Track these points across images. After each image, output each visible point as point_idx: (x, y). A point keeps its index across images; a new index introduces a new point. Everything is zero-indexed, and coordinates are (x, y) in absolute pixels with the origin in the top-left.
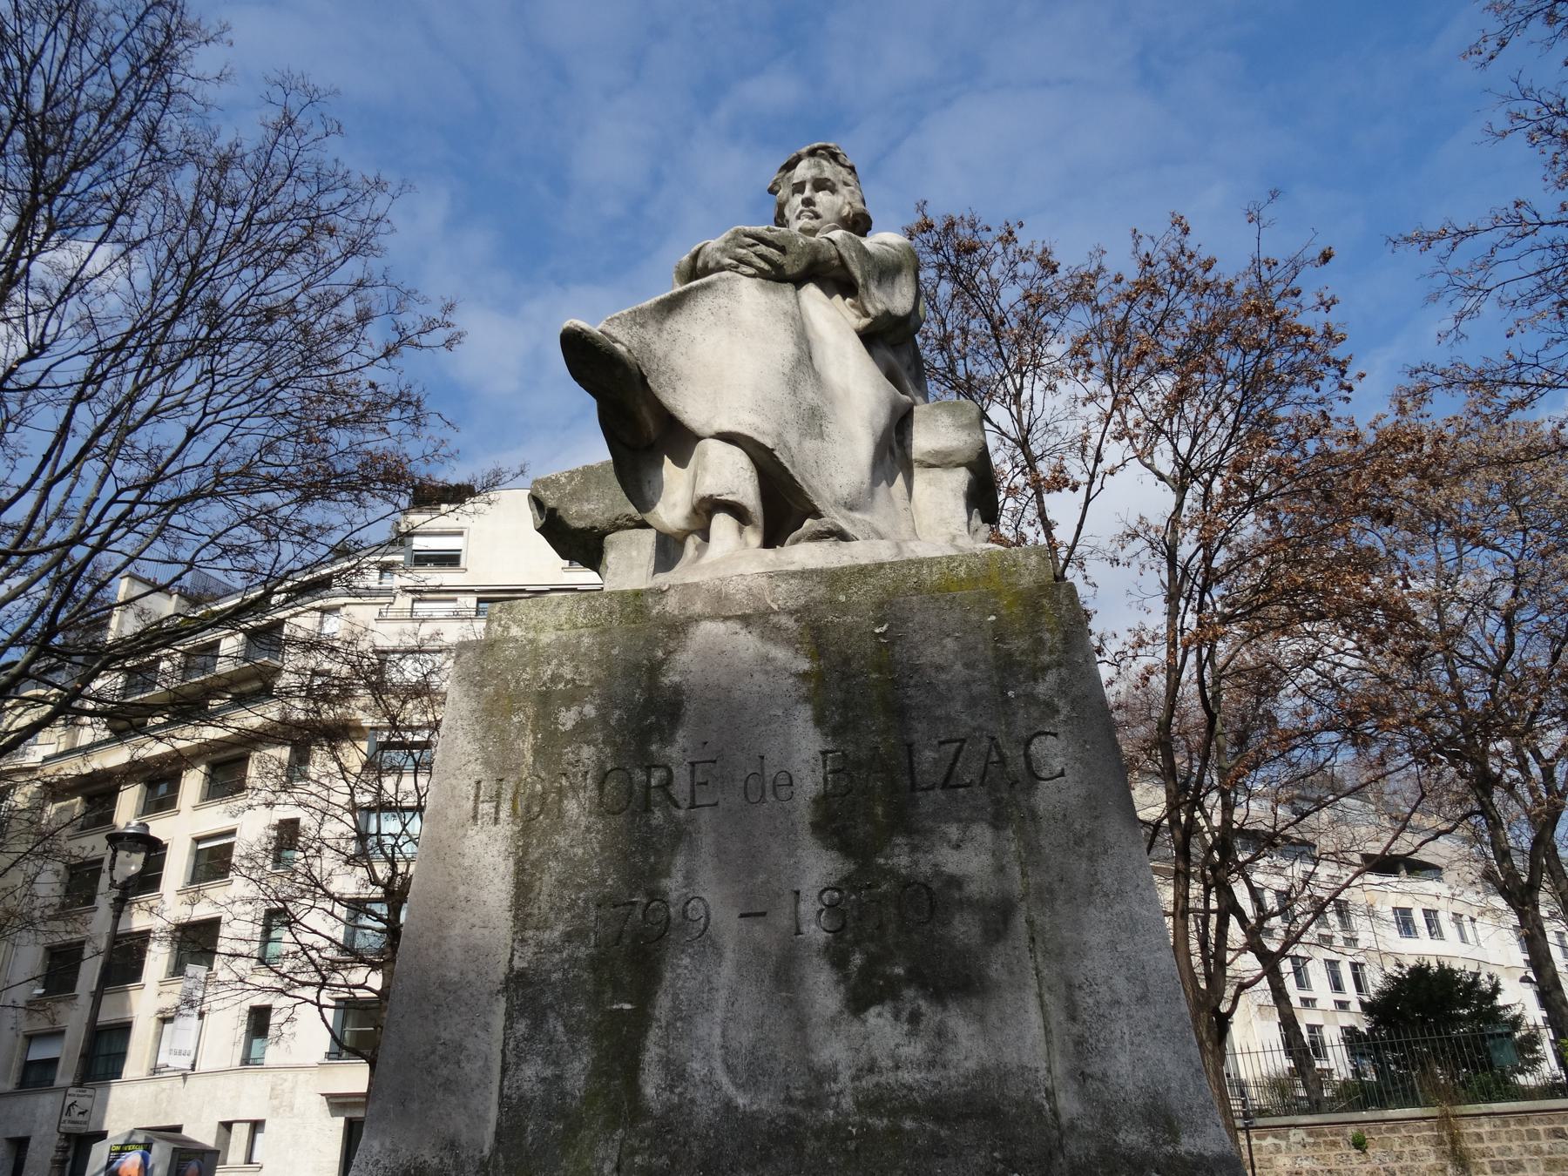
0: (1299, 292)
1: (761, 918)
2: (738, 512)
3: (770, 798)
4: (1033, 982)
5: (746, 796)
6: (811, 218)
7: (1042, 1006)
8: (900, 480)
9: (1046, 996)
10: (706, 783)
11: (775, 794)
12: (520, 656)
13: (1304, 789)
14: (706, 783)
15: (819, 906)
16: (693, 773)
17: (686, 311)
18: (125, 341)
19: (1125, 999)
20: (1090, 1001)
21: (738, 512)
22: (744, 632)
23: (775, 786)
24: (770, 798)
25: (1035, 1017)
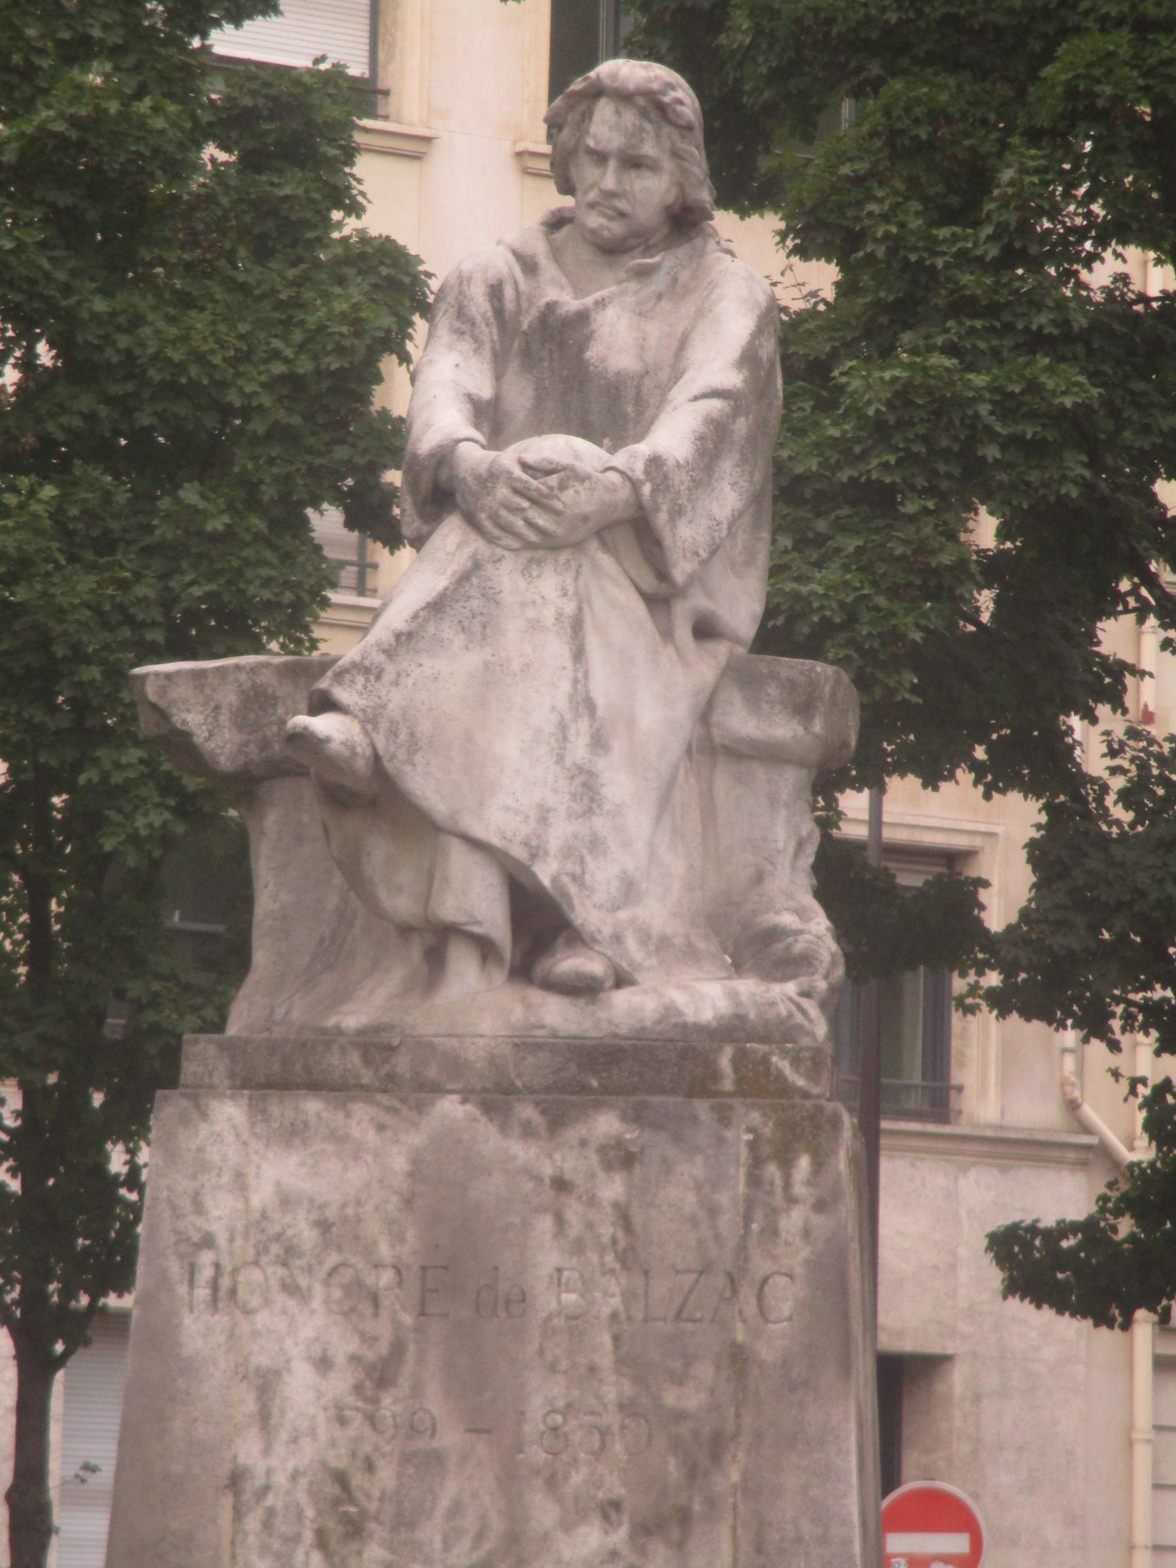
0: (1110, 1070)
1: (484, 1435)
2: (485, 947)
3: (502, 1314)
4: (729, 1517)
5: (478, 1309)
6: (611, 218)
7: (735, 1537)
8: (893, 1560)
9: (739, 1530)
10: (436, 1290)
11: (507, 1309)
12: (712, 1392)
13: (847, 556)
14: (436, 1290)
15: (542, 1428)
16: (423, 1278)
17: (469, 529)
18: (15, 529)
19: (807, 1538)
20: (777, 1537)
21: (485, 947)
22: (484, 1119)
23: (508, 1302)
24: (502, 1314)
25: (726, 1547)
